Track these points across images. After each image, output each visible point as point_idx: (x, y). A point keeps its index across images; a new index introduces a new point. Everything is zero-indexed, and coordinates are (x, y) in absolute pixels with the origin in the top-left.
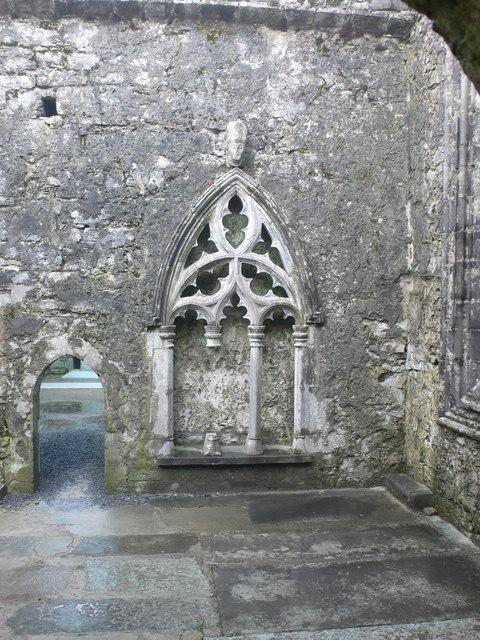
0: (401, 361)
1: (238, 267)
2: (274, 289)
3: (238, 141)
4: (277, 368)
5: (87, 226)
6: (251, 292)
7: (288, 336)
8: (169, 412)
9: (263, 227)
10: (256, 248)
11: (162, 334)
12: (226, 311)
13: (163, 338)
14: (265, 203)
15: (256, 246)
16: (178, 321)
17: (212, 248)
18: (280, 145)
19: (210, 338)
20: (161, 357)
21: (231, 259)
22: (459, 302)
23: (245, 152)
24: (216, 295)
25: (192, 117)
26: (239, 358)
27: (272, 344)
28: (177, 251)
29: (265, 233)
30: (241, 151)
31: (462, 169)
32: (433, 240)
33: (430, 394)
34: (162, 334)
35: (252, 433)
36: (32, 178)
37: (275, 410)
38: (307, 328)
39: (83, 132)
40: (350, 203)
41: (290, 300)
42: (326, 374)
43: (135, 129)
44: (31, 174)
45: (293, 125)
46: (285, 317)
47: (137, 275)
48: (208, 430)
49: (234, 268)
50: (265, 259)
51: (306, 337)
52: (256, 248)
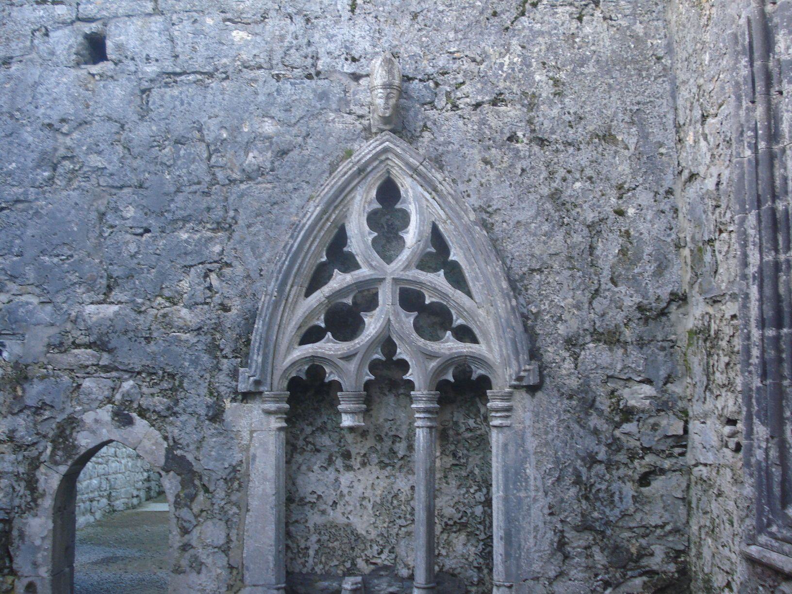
0: (677, 450)
1: (393, 292)
2: (452, 330)
3: (385, 86)
4: (465, 465)
5: (147, 231)
6: (415, 335)
7: (483, 410)
8: (278, 540)
9: (435, 229)
10: (426, 263)
11: (267, 406)
12: (374, 366)
13: (268, 413)
14: (435, 189)
15: (422, 261)
16: (294, 385)
17: (349, 263)
18: (459, 94)
19: (346, 412)
20: (263, 444)
21: (381, 280)
22: (770, 333)
23: (397, 108)
24: (356, 341)
25: (316, 58)
26: (401, 448)
27: (456, 423)
28: (290, 267)
29: (437, 237)
30: (392, 102)
31: (759, 98)
32: (721, 232)
33: (731, 506)
34: (267, 406)
35: (421, 577)
36: (65, 158)
37: (463, 537)
38: (511, 394)
39: (145, 85)
40: (578, 185)
41: (480, 349)
42: (549, 473)
43: (227, 78)
44: (62, 151)
45: (481, 63)
46: (474, 377)
47: (226, 309)
48: (349, 573)
49: (386, 296)
50: (439, 279)
51: (509, 409)
52: (426, 263)
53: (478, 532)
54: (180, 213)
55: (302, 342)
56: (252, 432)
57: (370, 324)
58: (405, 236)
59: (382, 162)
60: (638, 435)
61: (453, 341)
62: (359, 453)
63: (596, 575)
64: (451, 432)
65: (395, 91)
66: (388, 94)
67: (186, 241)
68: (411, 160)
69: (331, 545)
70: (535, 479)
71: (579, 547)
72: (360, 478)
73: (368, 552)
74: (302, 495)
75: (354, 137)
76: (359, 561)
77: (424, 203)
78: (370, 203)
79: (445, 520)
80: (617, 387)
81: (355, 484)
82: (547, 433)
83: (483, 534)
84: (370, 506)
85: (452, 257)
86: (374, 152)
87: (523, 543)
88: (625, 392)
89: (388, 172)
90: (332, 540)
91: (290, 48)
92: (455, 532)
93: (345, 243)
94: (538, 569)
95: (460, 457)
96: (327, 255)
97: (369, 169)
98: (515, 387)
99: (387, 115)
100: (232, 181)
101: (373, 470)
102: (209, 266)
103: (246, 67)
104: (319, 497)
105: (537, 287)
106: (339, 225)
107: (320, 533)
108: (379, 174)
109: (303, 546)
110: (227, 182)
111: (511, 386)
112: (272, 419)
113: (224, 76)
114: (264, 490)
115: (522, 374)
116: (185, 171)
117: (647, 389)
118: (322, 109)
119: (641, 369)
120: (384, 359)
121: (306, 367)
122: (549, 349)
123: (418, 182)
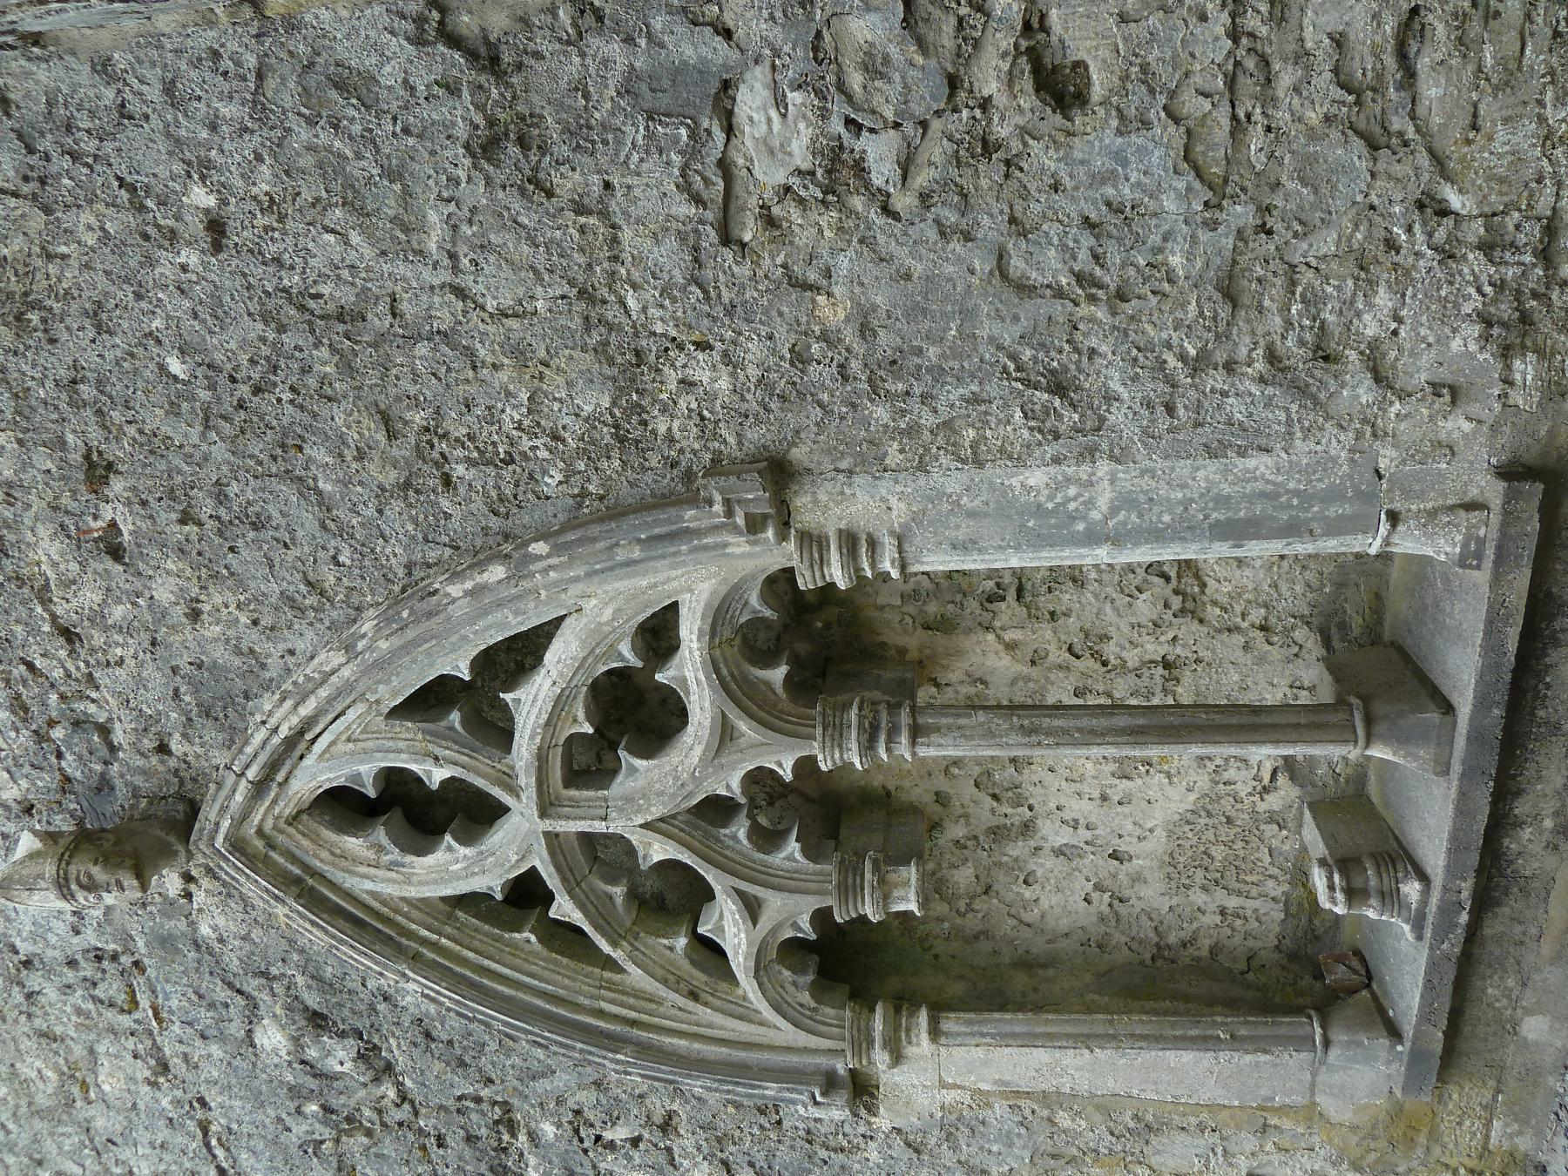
14: (290, 743)
56: (943, 1085)
59: (271, 845)
60: (909, 128)
61: (681, 667)
62: (993, 811)
63: (1391, 245)
64: (932, 608)
65: (73, 869)
66: (82, 886)
68: (239, 798)
70: (1057, 460)
72: (1052, 805)
73: (1243, 790)
74: (1094, 919)
76: (1262, 807)
78: (380, 849)
79: (1168, 616)
80: (753, 202)
81: (1067, 815)
82: (913, 431)
84: (1125, 784)
87: (1259, 485)
88: (771, 175)
89: (294, 819)
91: (95, 999)
92: (1203, 585)
93: (488, 896)
94: (1348, 438)
95: (998, 585)
97: (297, 871)
98: (784, 525)
100: (403, 1097)
101: (1035, 779)
104: (1098, 887)
105: (491, 470)
106: (447, 909)
107: (1187, 887)
108: (305, 843)
109: (1218, 919)
110: (406, 1106)
112: (911, 1051)
115: (740, 520)
117: (751, 101)
119: (683, 131)
121: (787, 973)
122: (662, 429)
123: (295, 766)
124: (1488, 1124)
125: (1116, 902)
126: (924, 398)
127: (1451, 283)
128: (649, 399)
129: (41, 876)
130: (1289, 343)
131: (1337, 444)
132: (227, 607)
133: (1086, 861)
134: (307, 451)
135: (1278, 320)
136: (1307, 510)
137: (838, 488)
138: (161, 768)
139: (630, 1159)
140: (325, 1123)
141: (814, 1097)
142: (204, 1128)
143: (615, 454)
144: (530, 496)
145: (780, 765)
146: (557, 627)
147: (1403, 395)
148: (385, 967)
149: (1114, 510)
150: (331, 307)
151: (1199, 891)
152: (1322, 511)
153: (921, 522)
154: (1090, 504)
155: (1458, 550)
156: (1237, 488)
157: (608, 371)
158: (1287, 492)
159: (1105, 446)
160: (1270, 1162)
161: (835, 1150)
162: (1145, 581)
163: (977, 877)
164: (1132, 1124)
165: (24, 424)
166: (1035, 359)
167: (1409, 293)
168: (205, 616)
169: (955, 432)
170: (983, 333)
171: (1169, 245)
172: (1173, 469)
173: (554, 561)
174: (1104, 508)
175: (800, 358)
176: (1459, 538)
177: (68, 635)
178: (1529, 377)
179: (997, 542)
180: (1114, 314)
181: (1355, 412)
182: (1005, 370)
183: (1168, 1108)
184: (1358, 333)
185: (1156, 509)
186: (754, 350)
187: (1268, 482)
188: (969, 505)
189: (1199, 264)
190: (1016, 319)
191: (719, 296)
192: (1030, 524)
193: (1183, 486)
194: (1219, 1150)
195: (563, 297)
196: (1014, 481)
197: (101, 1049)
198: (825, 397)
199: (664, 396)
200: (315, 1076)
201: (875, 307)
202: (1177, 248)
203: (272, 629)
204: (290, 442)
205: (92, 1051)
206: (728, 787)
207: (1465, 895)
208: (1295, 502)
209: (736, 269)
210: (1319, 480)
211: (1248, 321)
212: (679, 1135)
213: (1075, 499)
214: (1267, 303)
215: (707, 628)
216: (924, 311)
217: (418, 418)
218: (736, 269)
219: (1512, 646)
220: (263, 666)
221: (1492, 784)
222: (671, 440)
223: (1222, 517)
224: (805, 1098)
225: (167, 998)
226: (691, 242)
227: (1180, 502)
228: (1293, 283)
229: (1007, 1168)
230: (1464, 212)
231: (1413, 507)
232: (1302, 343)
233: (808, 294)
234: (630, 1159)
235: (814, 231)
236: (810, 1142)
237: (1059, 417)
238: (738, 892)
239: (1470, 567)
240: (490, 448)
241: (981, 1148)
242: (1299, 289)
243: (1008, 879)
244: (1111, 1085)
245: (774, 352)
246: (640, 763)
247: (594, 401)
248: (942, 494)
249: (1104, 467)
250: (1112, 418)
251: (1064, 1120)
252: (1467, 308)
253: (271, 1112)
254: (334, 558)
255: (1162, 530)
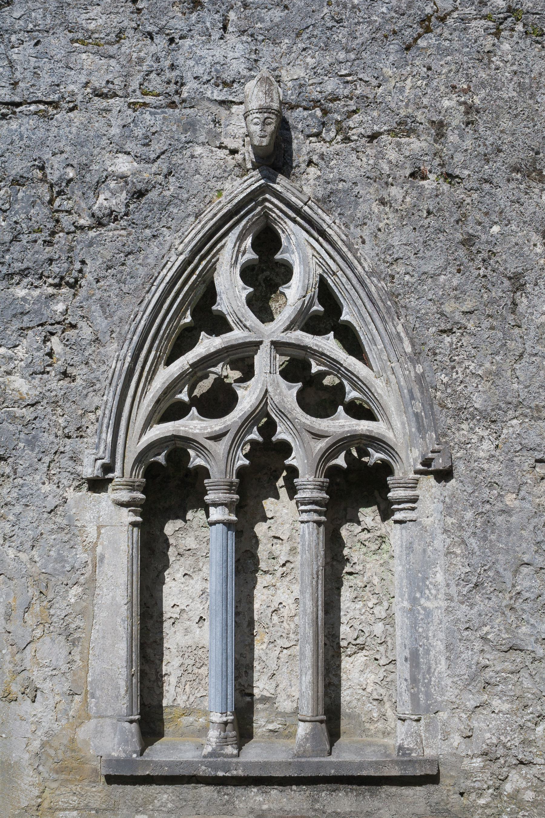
14: (322, 233)
53: (378, 657)
54: (18, 266)
55: (164, 419)
56: (99, 528)
57: (243, 397)
58: (286, 291)
66: (266, 119)
67: (24, 299)
69: (196, 671)
71: (503, 671)
75: (226, 175)
77: (310, 251)
83: (384, 657)
85: (345, 316)
86: (249, 190)
87: (434, 666)
89: (266, 216)
90: (198, 665)
93: (214, 302)
96: (192, 315)
99: (264, 144)
102: (49, 328)
103: (97, 95)
104: (183, 611)
110: (73, 229)
111: (416, 472)
113: (71, 105)
114: (113, 598)
115: (430, 455)
116: (23, 216)
118: (188, 143)
120: (260, 439)
122: (463, 426)
124: (75, 809)
125: (172, 620)
126: (474, 533)
127: (511, 731)
128: (476, 423)
129: (272, 101)
130: (491, 673)
131: (450, 694)
132: (388, 219)
133: (199, 605)
134: (458, 275)
135: (499, 669)
136: (422, 686)
137: (437, 497)
138: (301, 159)
139: (38, 349)
140: (60, 178)
141: (100, 459)
142: (55, 104)
143: (453, 406)
144: (436, 367)
145: (293, 459)
146: (365, 364)
147: (469, 718)
148: (187, 246)
149: (425, 609)
150: (518, 301)
151: (181, 662)
152: (421, 691)
153: (422, 530)
154: (428, 599)
155: (406, 746)
156: (432, 657)
157: (490, 408)
158: (431, 678)
159: (452, 604)
160: (47, 699)
161: (49, 467)
162: (355, 629)
163: (189, 550)
164: (73, 626)
165: (473, 154)
166: (489, 577)
167: (508, 716)
168: (382, 207)
169: (459, 545)
170: (500, 557)
171: (529, 626)
172: (442, 631)
173: (413, 374)
174: (425, 605)
175: (491, 486)
176: (411, 746)
177: (373, 137)
178: (474, 765)
179: (412, 560)
180: (506, 606)
181: (463, 700)
182: (485, 565)
183: (86, 645)
184: (493, 699)
185: (425, 626)
186: (495, 468)
187: (435, 670)
188: (428, 550)
189: (523, 637)
190: (505, 570)
191: (516, 456)
192: (420, 575)
193: (434, 636)
194: (54, 672)
195: (519, 395)
196: (438, 569)
197: (113, 62)
198: (476, 494)
199: (477, 429)
200: (98, 182)
201: (511, 516)
202: (528, 629)
203: (376, 236)
204: (462, 267)
205: (111, 57)
206: (280, 433)
207: (235, 773)
208: (426, 681)
209: (526, 464)
210: (435, 690)
211: (499, 657)
212: (60, 380)
213: (430, 593)
214: (506, 664)
215: (373, 434)
216: (509, 535)
217: (470, 326)
218: (526, 464)
219: (364, 773)
220: (357, 226)
221: (296, 775)
222: (459, 430)
223: (420, 652)
224: (101, 454)
225: (151, 113)
226: (537, 448)
227: (427, 635)
228: (512, 673)
229: (37, 560)
230: (536, 732)
231: (422, 728)
232: (491, 678)
233: (517, 491)
234: (38, 349)
235: (539, 495)
236: (55, 453)
237: (465, 586)
238: (227, 432)
239: (399, 752)
240: (457, 353)
241: (52, 546)
242: (510, 675)
243: (187, 566)
244: (102, 615)
245: (494, 475)
246: (294, 392)
247: (477, 401)
248: (433, 539)
249: (444, 604)
250: (464, 606)
251: (76, 590)
252: (502, 738)
253: (68, 149)
254: (408, 273)
255: (415, 628)
